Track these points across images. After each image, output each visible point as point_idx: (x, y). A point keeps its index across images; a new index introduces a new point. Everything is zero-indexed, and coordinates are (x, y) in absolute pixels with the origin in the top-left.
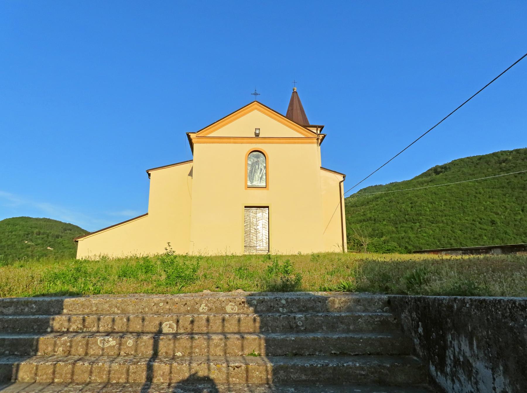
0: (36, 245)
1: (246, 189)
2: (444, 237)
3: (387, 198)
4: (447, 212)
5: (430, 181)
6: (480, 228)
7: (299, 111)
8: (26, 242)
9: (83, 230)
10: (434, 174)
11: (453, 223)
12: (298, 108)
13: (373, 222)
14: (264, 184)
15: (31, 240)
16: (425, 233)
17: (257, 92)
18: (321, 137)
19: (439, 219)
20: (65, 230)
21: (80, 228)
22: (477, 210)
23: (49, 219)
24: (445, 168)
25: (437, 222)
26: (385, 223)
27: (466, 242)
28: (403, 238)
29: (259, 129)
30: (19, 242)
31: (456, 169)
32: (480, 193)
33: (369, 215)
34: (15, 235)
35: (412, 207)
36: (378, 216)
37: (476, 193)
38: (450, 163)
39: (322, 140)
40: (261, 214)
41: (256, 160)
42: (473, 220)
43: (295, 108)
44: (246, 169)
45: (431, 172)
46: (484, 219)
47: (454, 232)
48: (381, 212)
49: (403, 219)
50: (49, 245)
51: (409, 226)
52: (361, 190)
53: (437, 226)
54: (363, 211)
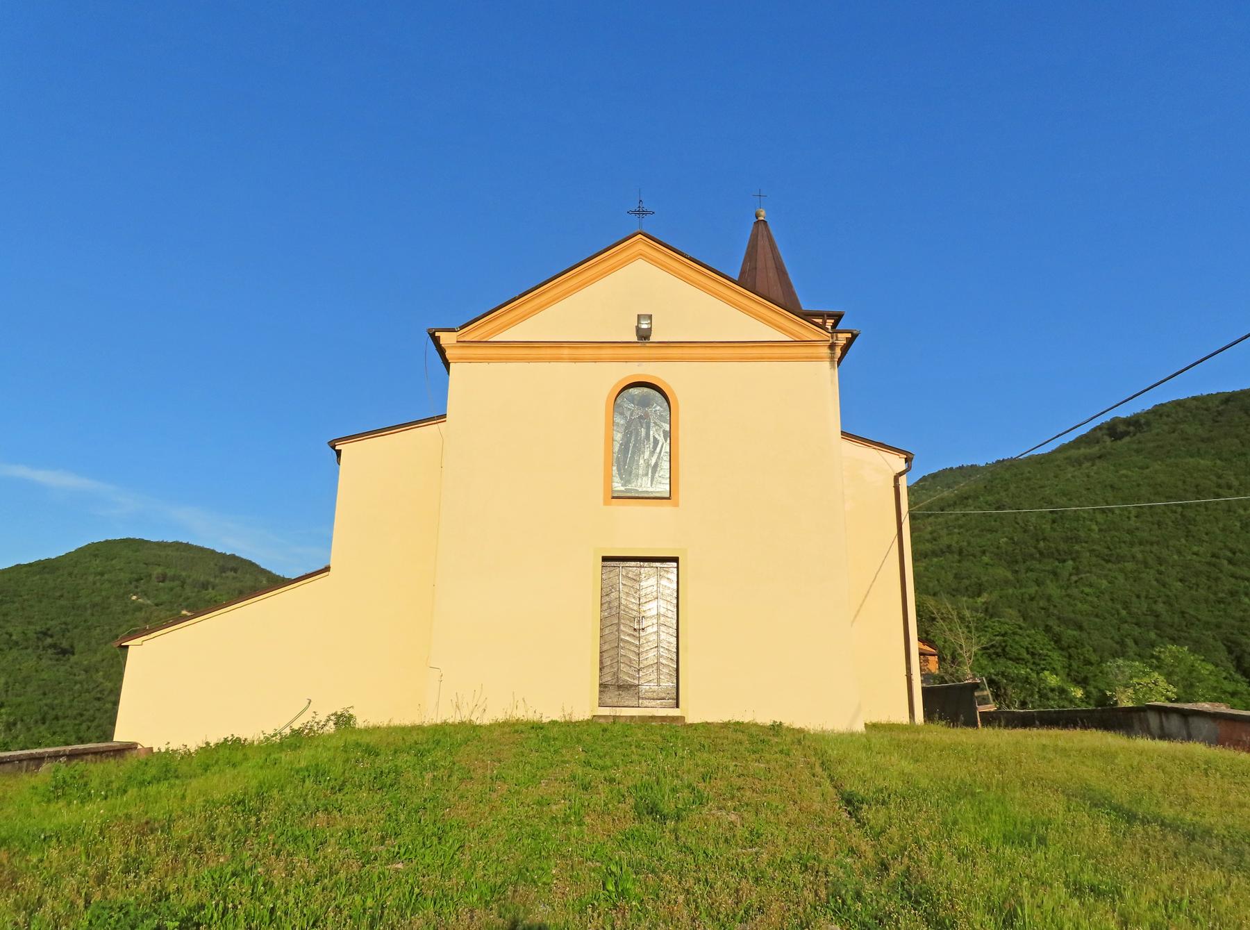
0: (157, 605)
1: (606, 503)
2: (1138, 597)
3: (989, 498)
4: (1145, 534)
5: (1100, 457)
6: (1233, 576)
7: (772, 274)
8: (134, 598)
9: (264, 572)
10: (1108, 440)
11: (1160, 561)
12: (771, 264)
13: (957, 557)
14: (663, 488)
15: (145, 594)
16: (1091, 586)
17: (646, 207)
18: (842, 339)
19: (1124, 550)
20: (223, 570)
21: (257, 566)
22: (1224, 530)
23: (187, 544)
24: (1135, 423)
25: (1120, 559)
26: (986, 559)
27: (1197, 610)
28: (1032, 599)
29: (650, 317)
30: (117, 597)
31: (1166, 428)
32: (1230, 487)
33: (945, 541)
34: (110, 581)
35: (1054, 522)
36: (969, 543)
37: (1219, 486)
38: (1148, 412)
39: (845, 349)
40: (653, 581)
41: (639, 412)
42: (1213, 555)
43: (760, 265)
44: (610, 440)
45: (1099, 434)
46: (1241, 552)
47: (1164, 586)
48: (976, 532)
49: (1033, 550)
50: (184, 604)
51: (1048, 568)
52: (924, 479)
53: (1121, 570)
54: (930, 529)
